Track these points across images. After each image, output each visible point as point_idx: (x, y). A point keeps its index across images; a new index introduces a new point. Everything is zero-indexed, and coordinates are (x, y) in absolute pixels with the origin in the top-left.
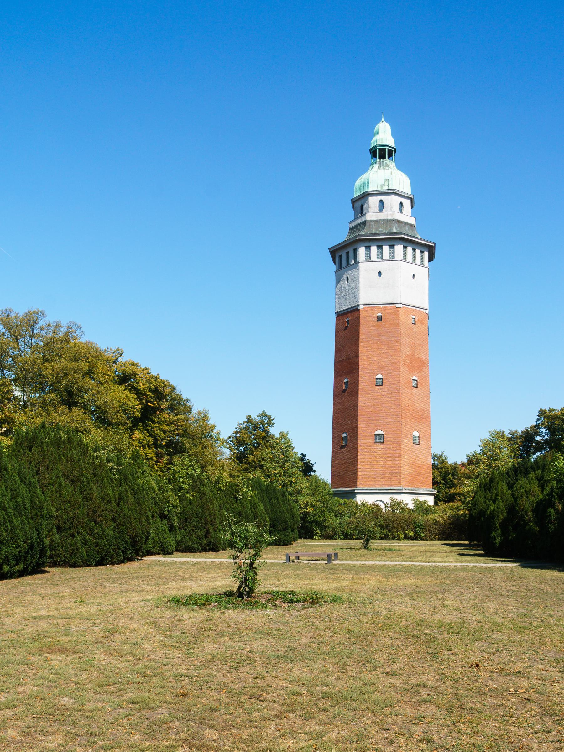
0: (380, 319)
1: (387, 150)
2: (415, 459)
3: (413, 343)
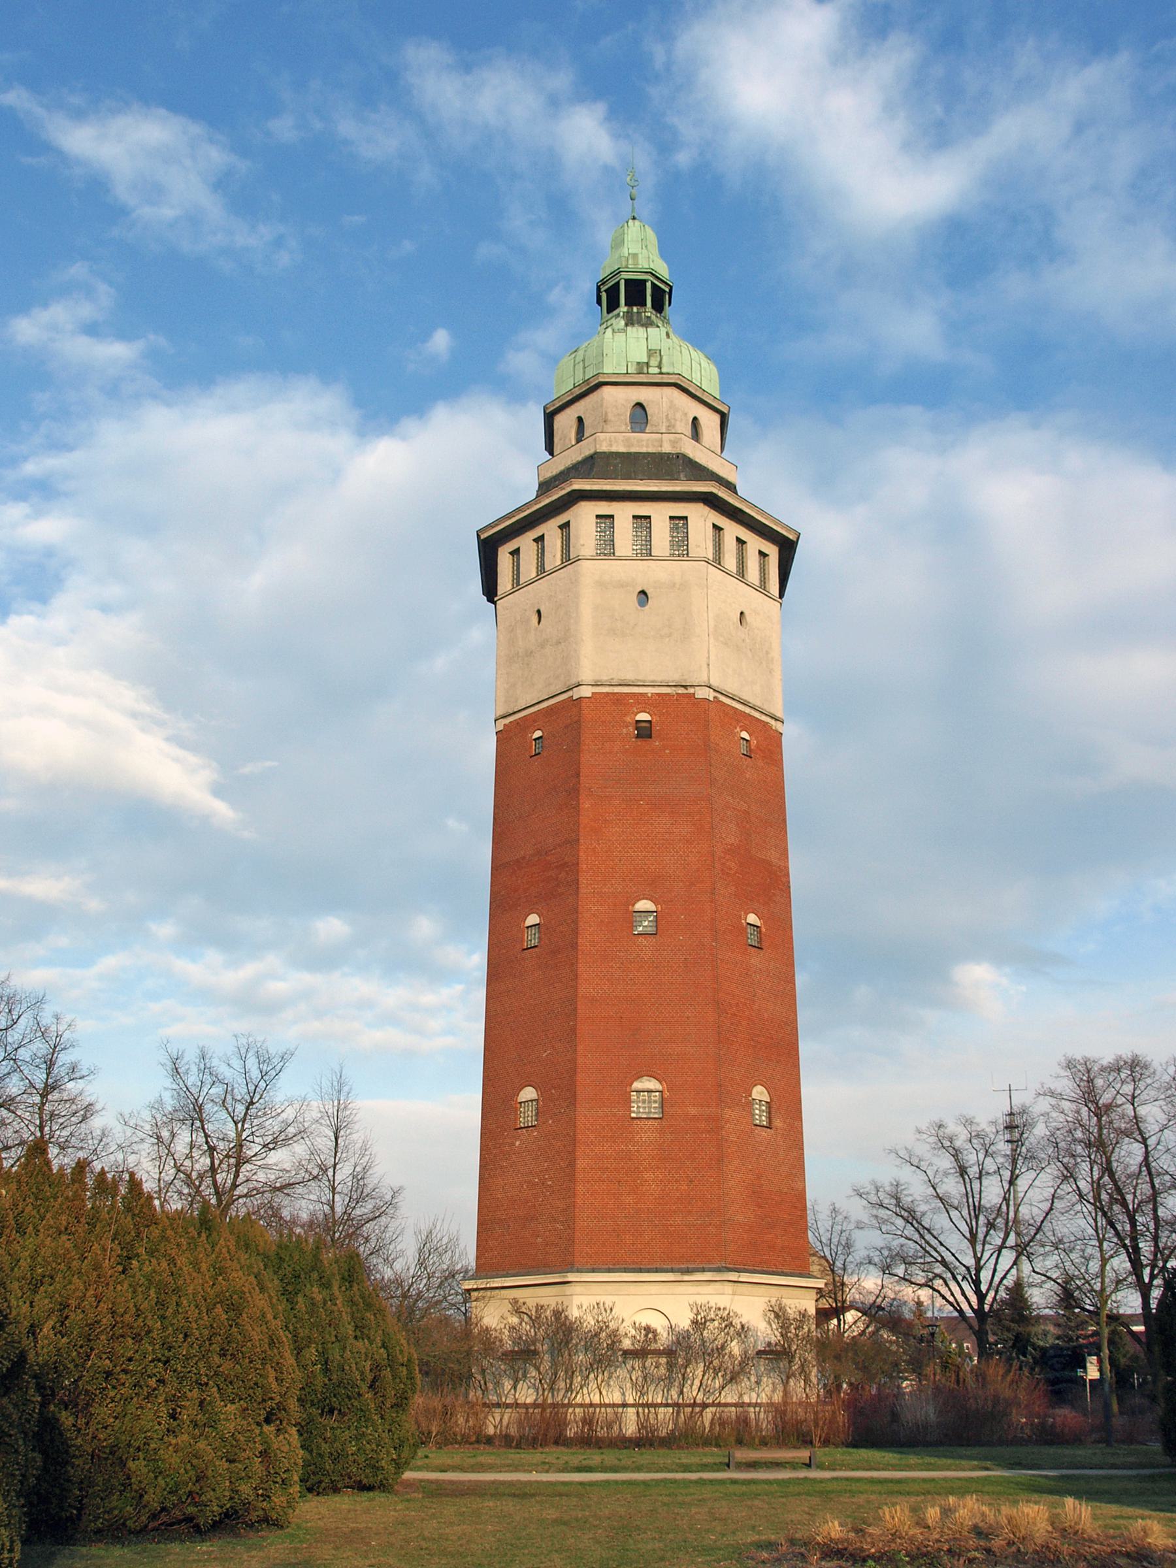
0: (644, 731)
1: (649, 285)
3: (747, 813)
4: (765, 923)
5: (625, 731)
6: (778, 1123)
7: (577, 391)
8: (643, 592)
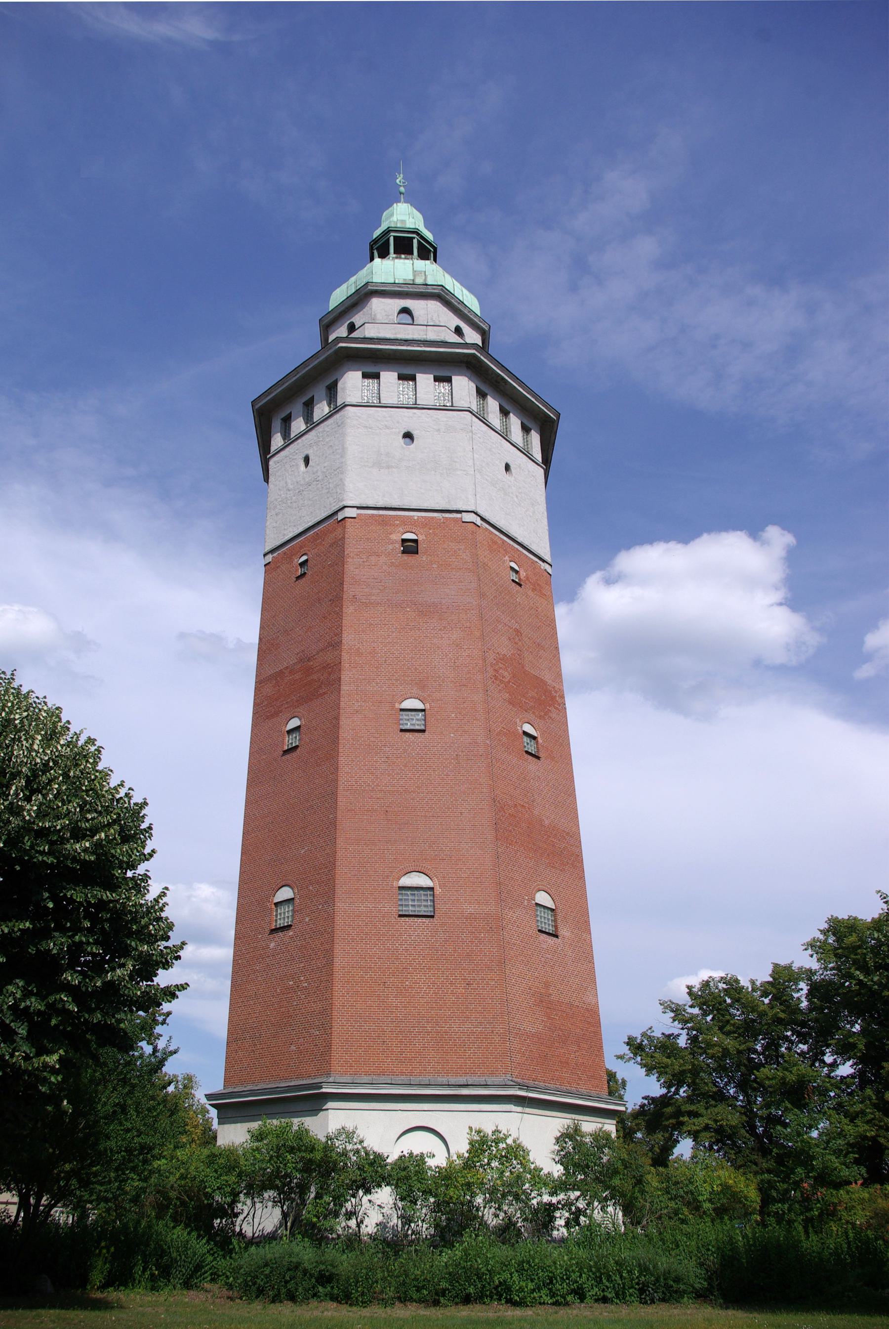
0: (410, 548)
2: (547, 985)
3: (518, 632)
4: (542, 734)
5: (391, 547)
6: (564, 932)
7: (349, 303)
8: (434, 1156)
